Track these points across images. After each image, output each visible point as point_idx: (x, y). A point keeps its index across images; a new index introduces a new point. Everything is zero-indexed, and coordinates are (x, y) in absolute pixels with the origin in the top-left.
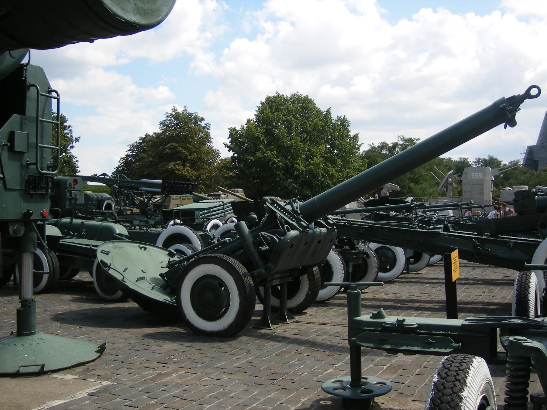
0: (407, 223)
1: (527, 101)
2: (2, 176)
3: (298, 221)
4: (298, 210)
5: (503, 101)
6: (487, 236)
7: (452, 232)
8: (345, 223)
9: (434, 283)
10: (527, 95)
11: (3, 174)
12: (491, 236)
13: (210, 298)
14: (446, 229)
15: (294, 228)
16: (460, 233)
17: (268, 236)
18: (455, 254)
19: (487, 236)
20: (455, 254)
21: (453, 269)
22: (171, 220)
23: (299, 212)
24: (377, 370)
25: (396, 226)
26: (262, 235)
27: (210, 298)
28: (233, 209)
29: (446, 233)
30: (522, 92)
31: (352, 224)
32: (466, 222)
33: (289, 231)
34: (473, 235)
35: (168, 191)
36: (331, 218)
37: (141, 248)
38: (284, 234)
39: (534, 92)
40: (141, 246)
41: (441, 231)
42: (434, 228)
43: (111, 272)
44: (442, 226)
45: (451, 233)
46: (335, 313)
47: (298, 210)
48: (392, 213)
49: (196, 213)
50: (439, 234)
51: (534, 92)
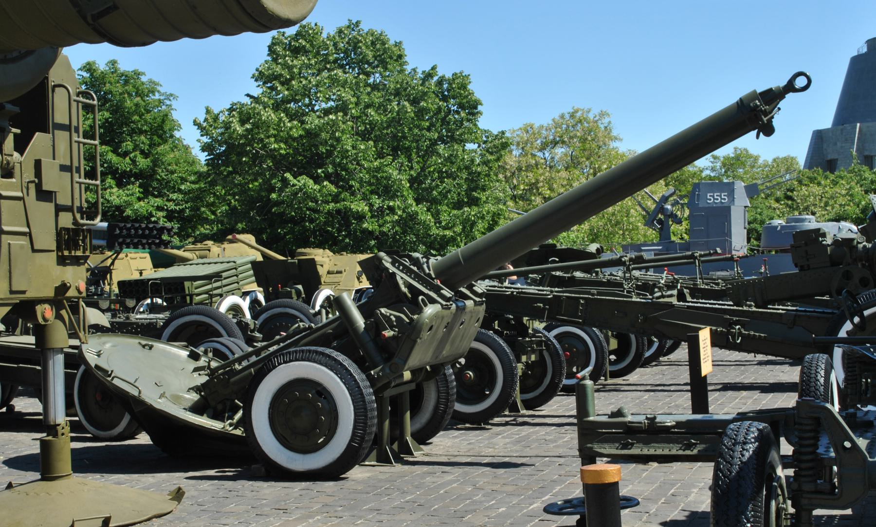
0: (616, 290)
1: (790, 96)
2: (27, 230)
3: (437, 290)
4: (432, 273)
5: (754, 96)
6: (750, 306)
7: (690, 302)
8: (512, 292)
9: (664, 385)
10: (790, 87)
11: (28, 226)
12: (756, 307)
13: (302, 416)
14: (681, 297)
15: (433, 301)
16: (706, 303)
17: (391, 314)
18: (705, 335)
19: (750, 306)
20: (705, 335)
21: (702, 357)
22: (145, 298)
23: (433, 276)
24: (629, 479)
25: (599, 294)
26: (381, 313)
27: (302, 416)
28: (255, 275)
29: (681, 303)
30: (783, 83)
31: (522, 293)
32: (707, 284)
33: (426, 305)
34: (727, 304)
35: (121, 245)
36: (481, 286)
37: (144, 346)
38: (420, 311)
39: (801, 82)
40: (144, 342)
41: (674, 301)
42: (663, 296)
43: (116, 382)
44: (675, 292)
45: (690, 304)
46: (507, 440)
47: (432, 273)
48: (578, 274)
49: (187, 284)
50: (671, 305)
51: (801, 82)
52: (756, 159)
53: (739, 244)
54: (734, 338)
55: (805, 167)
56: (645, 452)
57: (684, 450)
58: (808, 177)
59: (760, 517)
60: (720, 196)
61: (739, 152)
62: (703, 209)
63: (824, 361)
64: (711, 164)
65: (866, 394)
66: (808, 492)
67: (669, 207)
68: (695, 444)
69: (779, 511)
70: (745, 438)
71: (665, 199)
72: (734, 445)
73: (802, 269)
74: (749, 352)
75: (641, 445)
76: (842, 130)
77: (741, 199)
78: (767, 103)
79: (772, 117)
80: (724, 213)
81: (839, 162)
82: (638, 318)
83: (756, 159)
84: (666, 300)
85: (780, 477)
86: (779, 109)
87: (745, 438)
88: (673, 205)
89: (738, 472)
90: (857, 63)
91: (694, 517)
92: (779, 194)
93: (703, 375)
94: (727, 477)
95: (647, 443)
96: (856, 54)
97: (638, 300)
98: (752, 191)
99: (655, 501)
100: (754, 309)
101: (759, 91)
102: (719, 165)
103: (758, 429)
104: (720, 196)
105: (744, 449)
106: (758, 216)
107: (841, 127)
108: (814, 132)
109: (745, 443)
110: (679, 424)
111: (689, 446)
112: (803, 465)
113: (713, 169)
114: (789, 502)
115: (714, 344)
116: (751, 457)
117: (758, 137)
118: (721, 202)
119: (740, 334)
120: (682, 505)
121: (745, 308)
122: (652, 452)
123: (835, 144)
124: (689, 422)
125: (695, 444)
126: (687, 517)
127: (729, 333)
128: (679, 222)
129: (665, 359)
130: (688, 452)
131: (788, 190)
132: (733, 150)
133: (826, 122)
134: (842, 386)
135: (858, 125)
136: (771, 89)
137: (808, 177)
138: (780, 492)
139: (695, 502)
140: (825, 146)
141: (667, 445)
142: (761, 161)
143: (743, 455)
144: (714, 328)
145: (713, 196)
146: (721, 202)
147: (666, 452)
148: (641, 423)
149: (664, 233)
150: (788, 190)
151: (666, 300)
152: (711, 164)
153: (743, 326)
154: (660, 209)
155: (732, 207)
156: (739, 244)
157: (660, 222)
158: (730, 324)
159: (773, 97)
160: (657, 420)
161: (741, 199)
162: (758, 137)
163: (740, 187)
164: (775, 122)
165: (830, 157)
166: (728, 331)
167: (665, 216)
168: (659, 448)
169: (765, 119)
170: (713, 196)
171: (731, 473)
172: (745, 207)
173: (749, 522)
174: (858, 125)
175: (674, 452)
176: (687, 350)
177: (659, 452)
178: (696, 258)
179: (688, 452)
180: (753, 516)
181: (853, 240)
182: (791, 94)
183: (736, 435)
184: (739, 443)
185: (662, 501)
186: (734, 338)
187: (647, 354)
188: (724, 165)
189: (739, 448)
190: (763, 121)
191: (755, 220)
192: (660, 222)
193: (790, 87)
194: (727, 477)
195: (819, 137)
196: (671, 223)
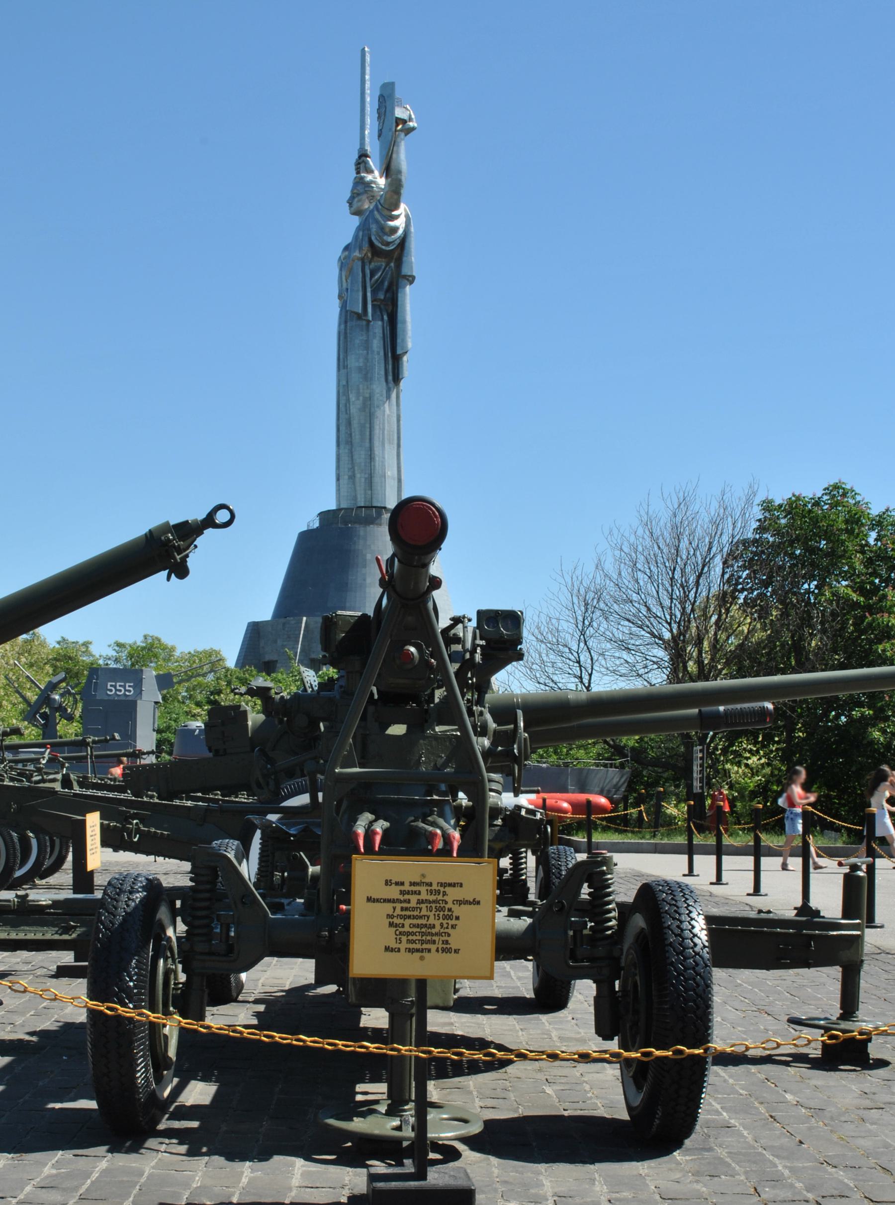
1: (209, 532)
5: (166, 528)
6: (152, 797)
10: (209, 522)
18: (93, 821)
21: (89, 847)
30: (201, 515)
32: (102, 780)
41: (57, 787)
42: (43, 781)
50: (53, 792)
51: (222, 516)
52: (173, 649)
53: (146, 740)
54: (129, 835)
55: (236, 666)
56: (13, 936)
57: (61, 935)
58: (237, 678)
59: (145, 976)
60: (124, 687)
61: (150, 641)
62: (101, 702)
63: (234, 847)
64: (114, 654)
65: (282, 889)
66: (202, 954)
67: (57, 697)
68: (75, 927)
69: (167, 973)
70: (132, 888)
71: (52, 687)
72: (118, 894)
73: (217, 753)
74: (148, 854)
75: (8, 928)
76: (284, 624)
77: (151, 693)
78: (182, 538)
79: (187, 556)
80: (126, 711)
81: (278, 665)
82: (11, 807)
83: (173, 649)
84: (47, 785)
85: (170, 938)
86: (196, 546)
87: (132, 888)
88: (62, 695)
89: (121, 924)
90: (306, 538)
91: (69, 1028)
92: (199, 698)
93: (89, 869)
94: (109, 929)
95: (15, 925)
96: (305, 529)
97: (11, 784)
98: (164, 681)
99: (23, 1014)
100: (156, 801)
101: (172, 523)
102: (124, 655)
103: (147, 879)
104: (124, 687)
105: (129, 899)
106: (173, 723)
107: (283, 620)
108: (249, 623)
109: (131, 892)
110: (56, 904)
111: (67, 930)
112: (197, 923)
113: (117, 660)
114: (180, 967)
115: (105, 843)
116: (136, 907)
117: (169, 579)
118: (125, 694)
119: (138, 831)
120: (56, 1016)
121: (145, 799)
122: (21, 936)
123: (275, 642)
124: (67, 901)
125: (75, 927)
126: (60, 1027)
127: (124, 829)
128: (70, 718)
129: (44, 882)
130: (66, 937)
131: (212, 693)
132: (142, 638)
133: (265, 612)
134: (245, 860)
135: (305, 619)
136: (187, 521)
137: (237, 678)
138: (169, 954)
139: (71, 1014)
140: (262, 644)
141: (40, 929)
142: (177, 654)
143: (128, 906)
144: (106, 822)
145: (115, 687)
146: (125, 694)
147: (39, 936)
148: (9, 901)
149: (48, 728)
150: (212, 693)
151: (47, 785)
152: (114, 654)
153: (142, 820)
154: (45, 698)
155: (139, 702)
156: (146, 740)
157: (44, 716)
158: (127, 818)
159: (188, 532)
160: (30, 898)
161: (151, 693)
162: (169, 579)
163: (150, 674)
164: (190, 562)
165: (267, 658)
166: (124, 826)
167: (50, 709)
168: (30, 931)
169: (178, 557)
170: (115, 687)
171: (113, 925)
172: (156, 703)
173: (131, 980)
174: (305, 619)
175: (48, 936)
176: (71, 875)
177: (31, 936)
178: (88, 744)
179: (66, 937)
180: (136, 974)
181: (269, 689)
182: (210, 529)
183: (121, 884)
184: (125, 892)
185: (32, 1013)
186: (129, 835)
187: (18, 874)
188: (131, 656)
189: (124, 898)
190: (175, 558)
191: (168, 728)
192: (44, 716)
193: (209, 522)
194: (109, 929)
195: (255, 631)
196: (58, 718)
